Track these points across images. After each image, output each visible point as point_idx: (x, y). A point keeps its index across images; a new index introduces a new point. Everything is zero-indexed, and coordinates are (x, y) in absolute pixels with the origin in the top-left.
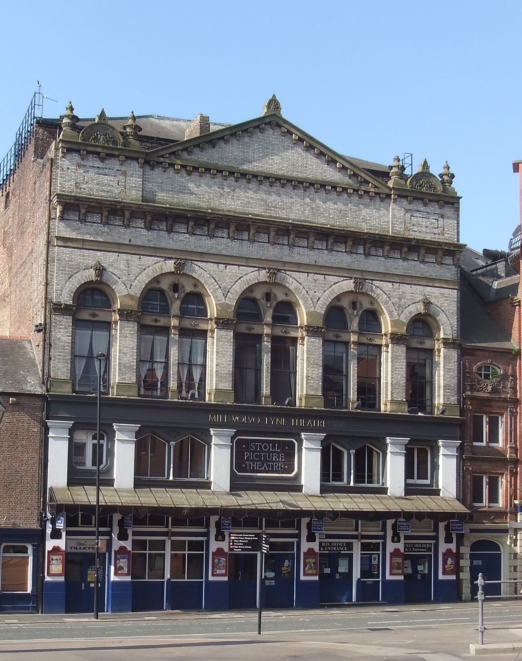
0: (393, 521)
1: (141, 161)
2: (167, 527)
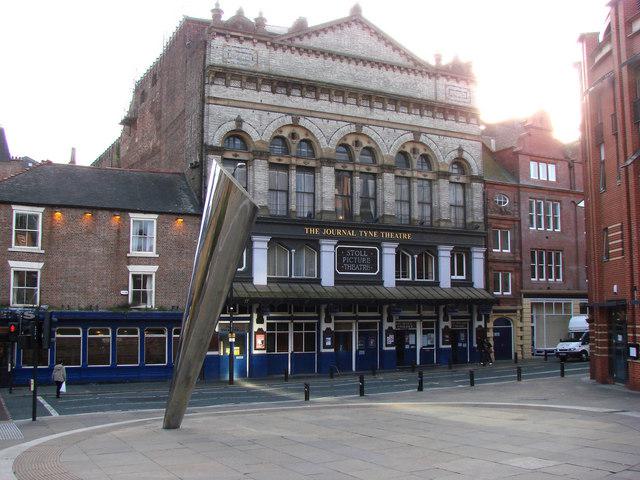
0: (443, 306)
1: (269, 43)
2: (355, 312)
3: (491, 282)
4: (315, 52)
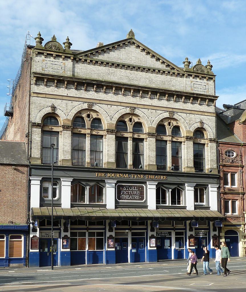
3: (223, 205)
4: (107, 64)
